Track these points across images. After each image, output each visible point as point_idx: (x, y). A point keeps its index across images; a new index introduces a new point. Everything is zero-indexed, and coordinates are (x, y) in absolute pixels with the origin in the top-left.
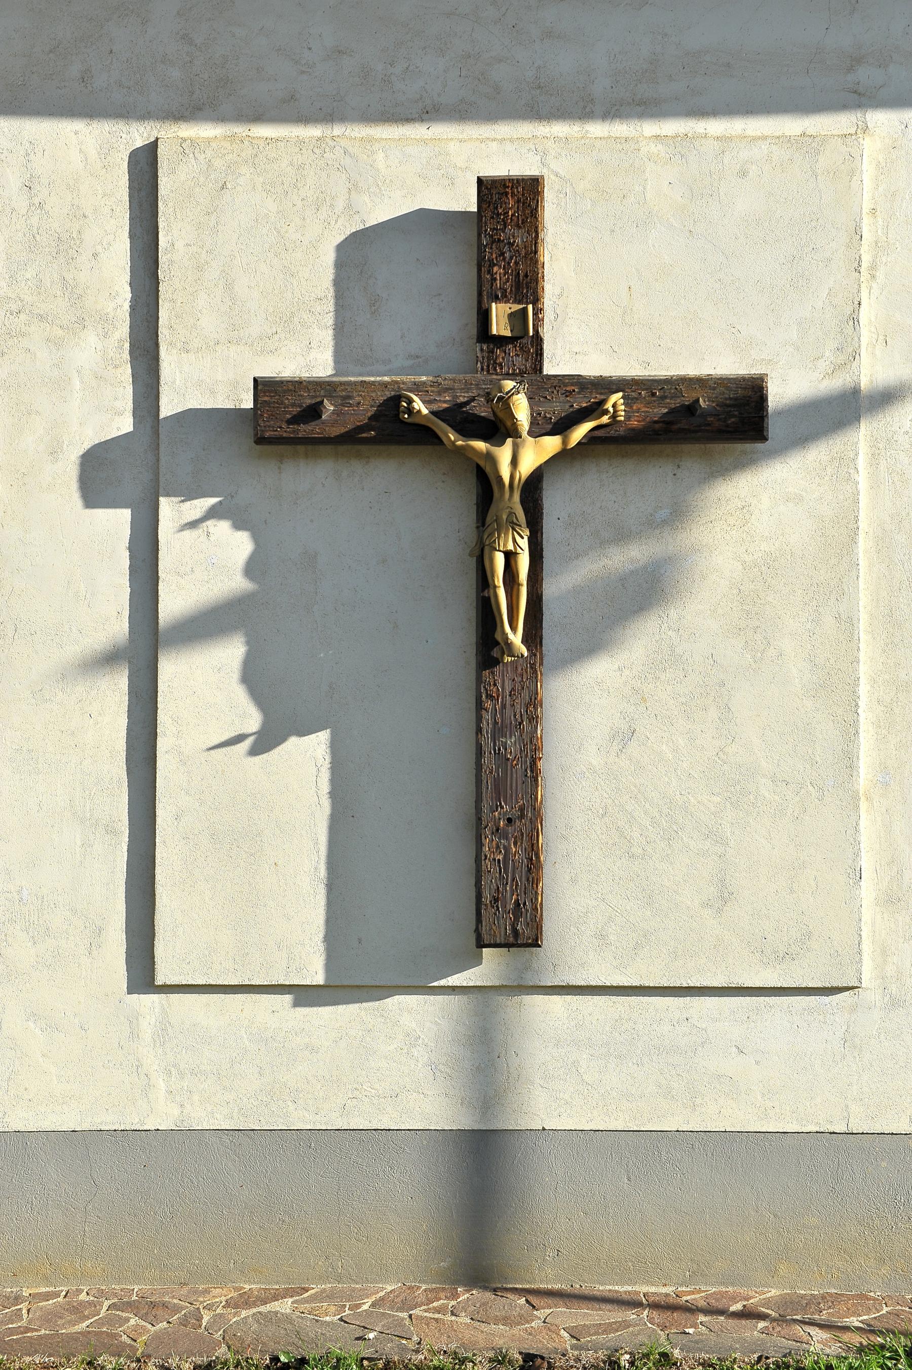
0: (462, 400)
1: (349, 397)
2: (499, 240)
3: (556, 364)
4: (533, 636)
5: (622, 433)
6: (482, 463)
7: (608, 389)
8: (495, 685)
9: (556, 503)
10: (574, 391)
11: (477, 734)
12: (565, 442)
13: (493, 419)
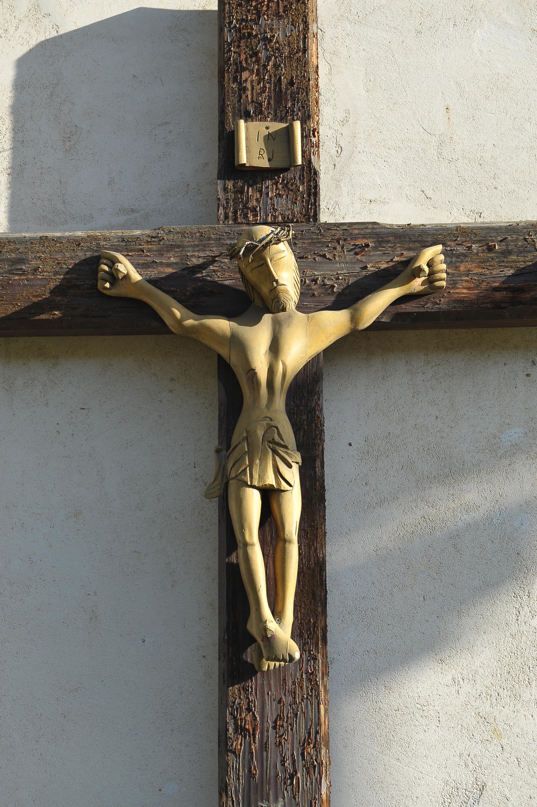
0: (195, 261)
1: (21, 261)
2: (250, 34)
3: (338, 205)
4: (311, 626)
5: (444, 307)
6: (224, 352)
7: (420, 242)
8: (249, 709)
9: (343, 413)
10: (367, 246)
11: (220, 795)
12: (354, 319)
13: (243, 288)
